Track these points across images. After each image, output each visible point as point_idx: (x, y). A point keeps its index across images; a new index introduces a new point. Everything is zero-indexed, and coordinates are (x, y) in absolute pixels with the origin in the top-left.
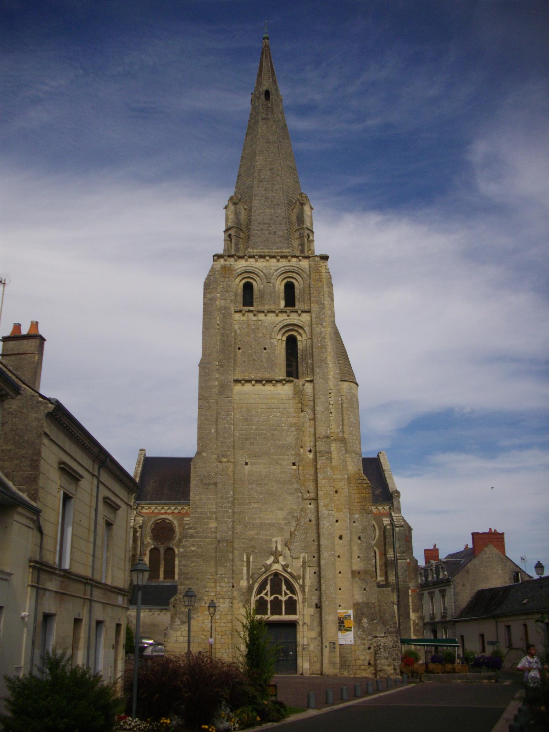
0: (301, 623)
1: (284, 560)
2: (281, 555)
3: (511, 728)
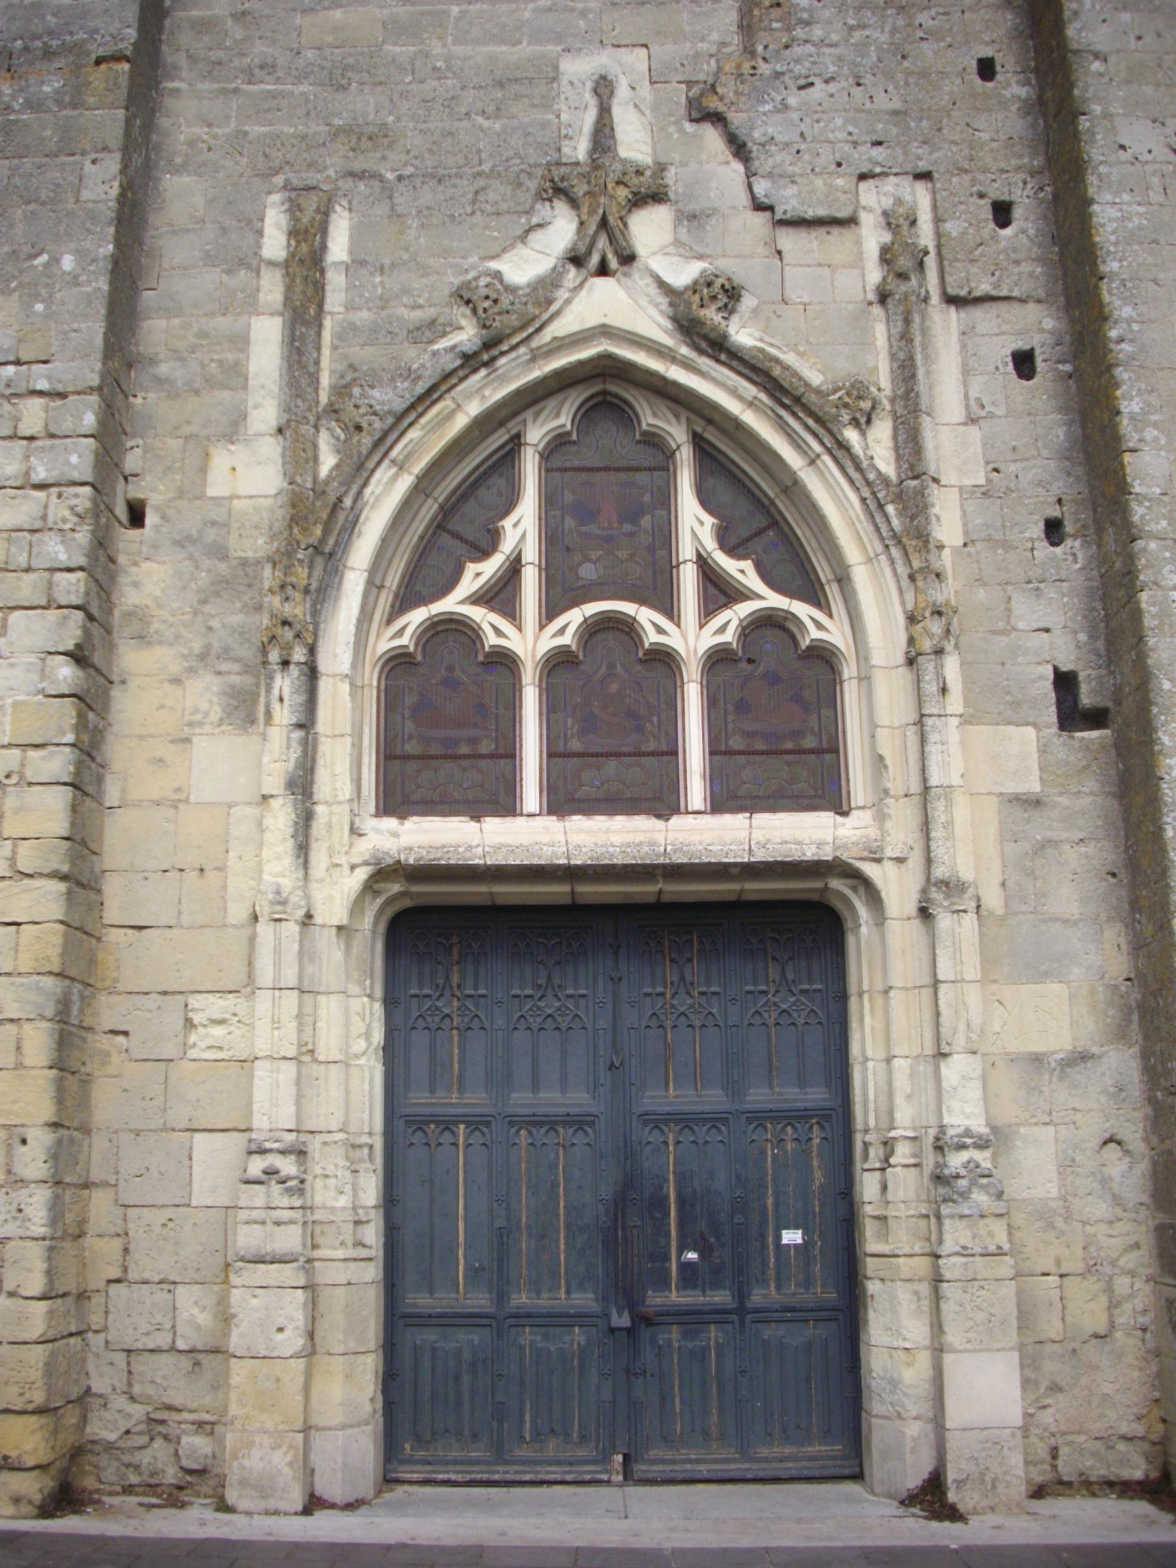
0: (898, 887)
1: (683, 249)
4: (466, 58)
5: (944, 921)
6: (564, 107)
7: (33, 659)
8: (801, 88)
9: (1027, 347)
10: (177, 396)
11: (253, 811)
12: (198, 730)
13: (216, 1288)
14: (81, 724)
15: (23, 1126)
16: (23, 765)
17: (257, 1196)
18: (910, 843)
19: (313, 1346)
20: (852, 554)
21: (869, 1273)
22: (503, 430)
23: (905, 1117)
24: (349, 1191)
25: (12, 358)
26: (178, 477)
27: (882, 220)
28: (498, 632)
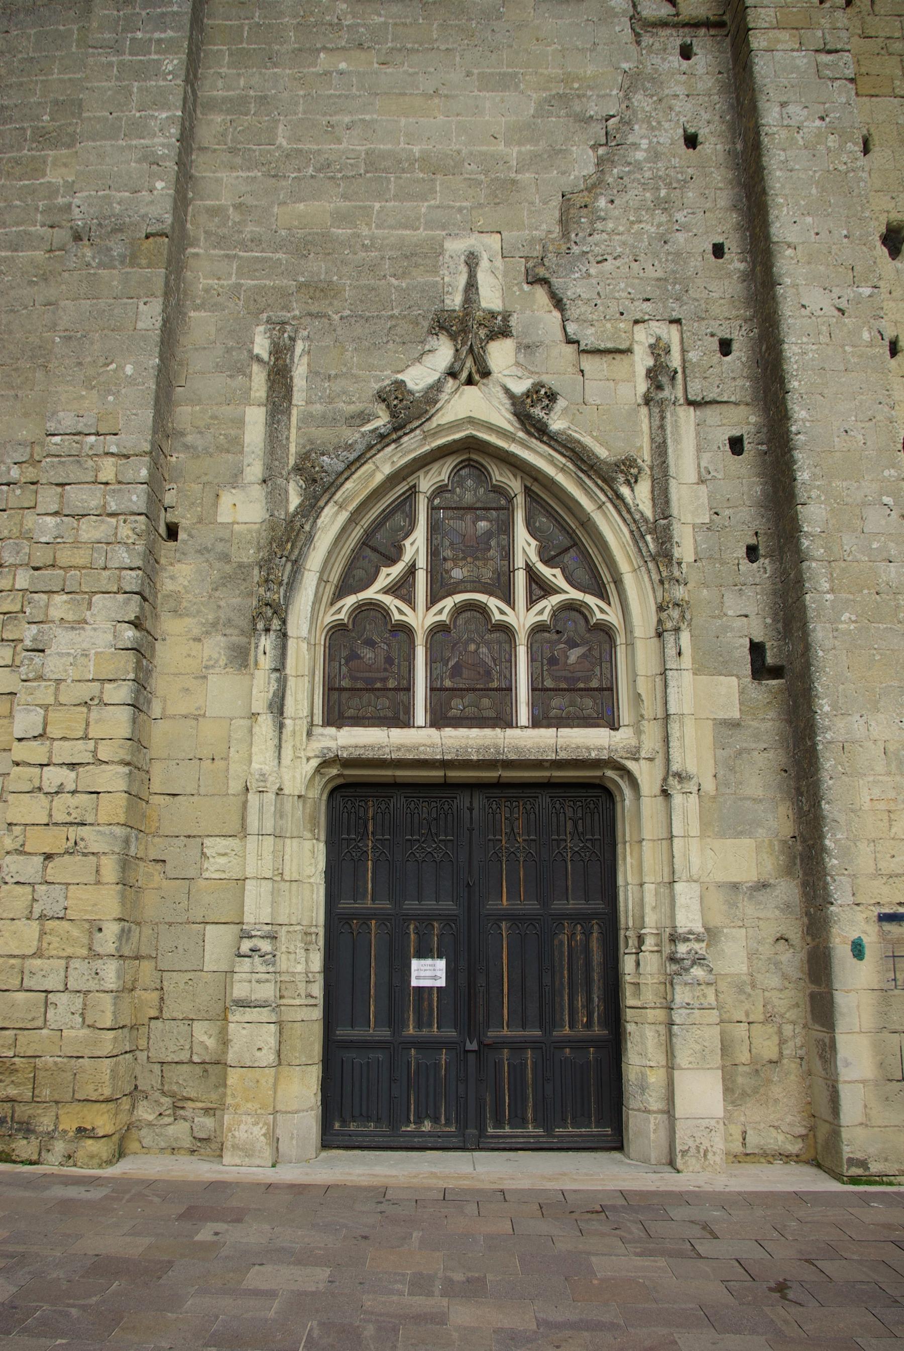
0: (647, 775)
2: (504, 332)
3: (3, 1151)
4: (384, 239)
5: (678, 799)
6: (446, 273)
7: (109, 625)
8: (598, 263)
9: (739, 434)
10: (198, 457)
11: (246, 723)
12: (211, 671)
13: (219, 1023)
14: (138, 667)
15: (100, 920)
16: (102, 693)
17: (245, 965)
18: (657, 749)
19: (280, 1059)
20: (624, 567)
21: (628, 1019)
22: (405, 483)
23: (651, 919)
24: (305, 963)
25: (93, 431)
26: (199, 509)
27: (648, 350)
28: (400, 611)
